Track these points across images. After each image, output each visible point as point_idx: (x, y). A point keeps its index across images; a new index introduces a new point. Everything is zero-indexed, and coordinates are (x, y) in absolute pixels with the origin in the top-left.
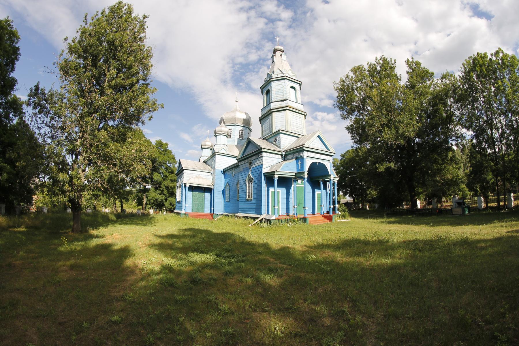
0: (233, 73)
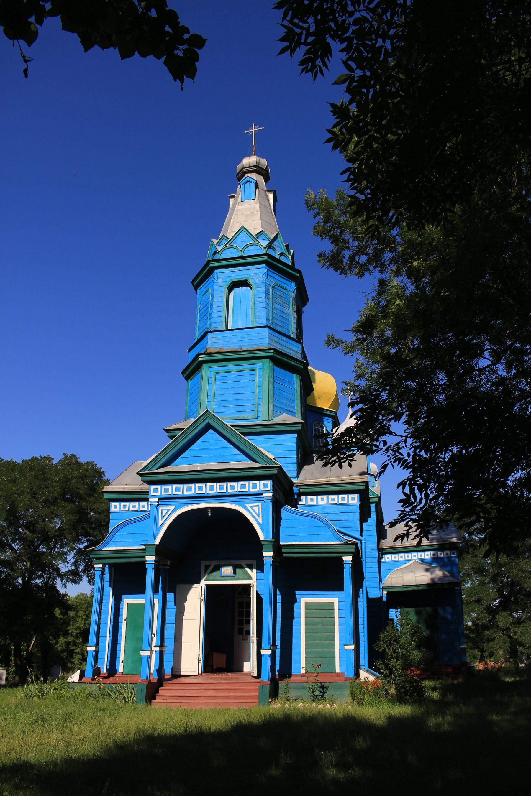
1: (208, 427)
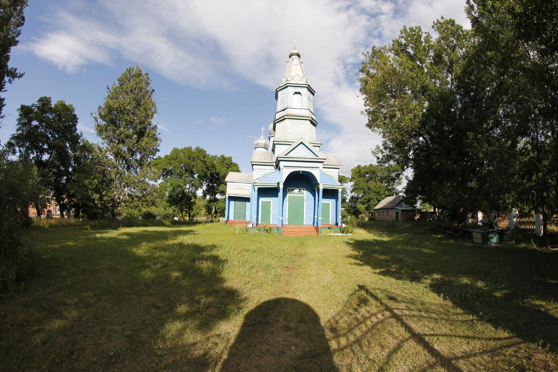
0: (346, 74)
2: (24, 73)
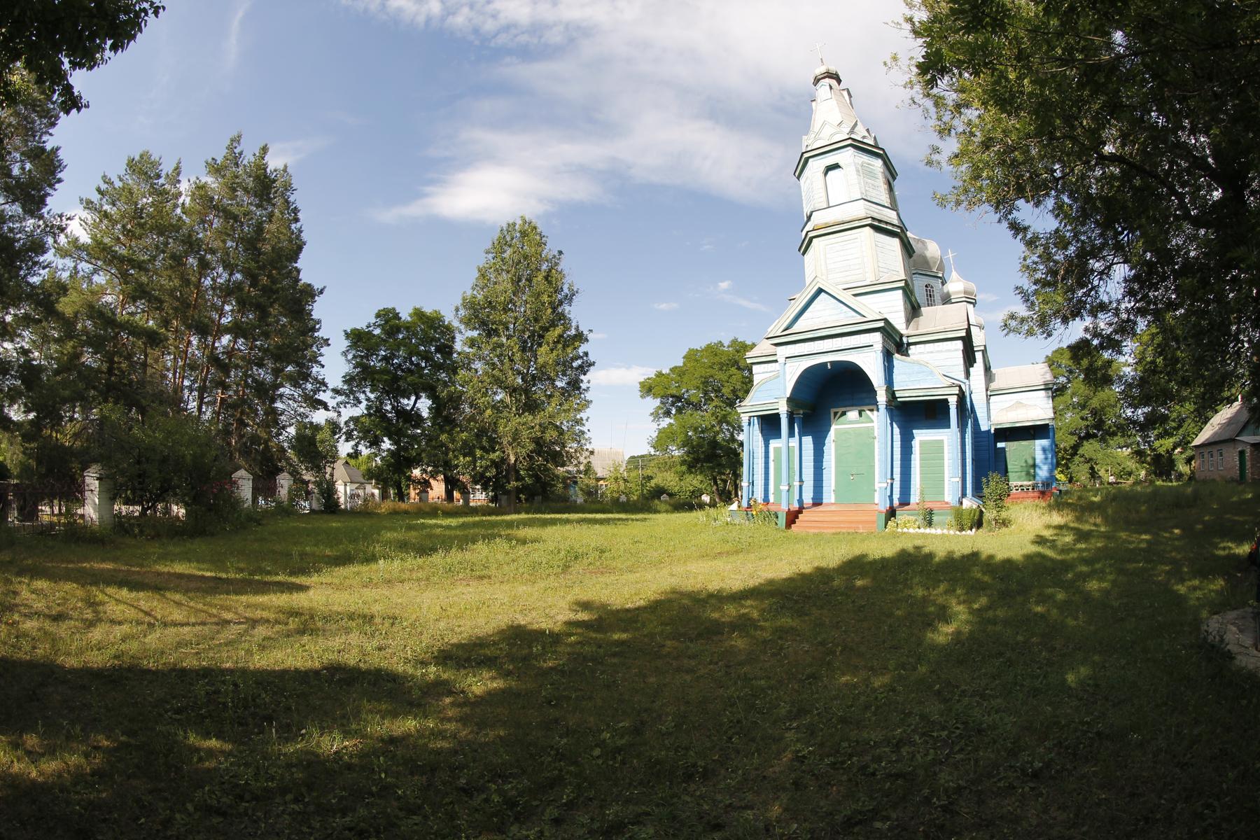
1: (820, 291)
2: (325, 287)
